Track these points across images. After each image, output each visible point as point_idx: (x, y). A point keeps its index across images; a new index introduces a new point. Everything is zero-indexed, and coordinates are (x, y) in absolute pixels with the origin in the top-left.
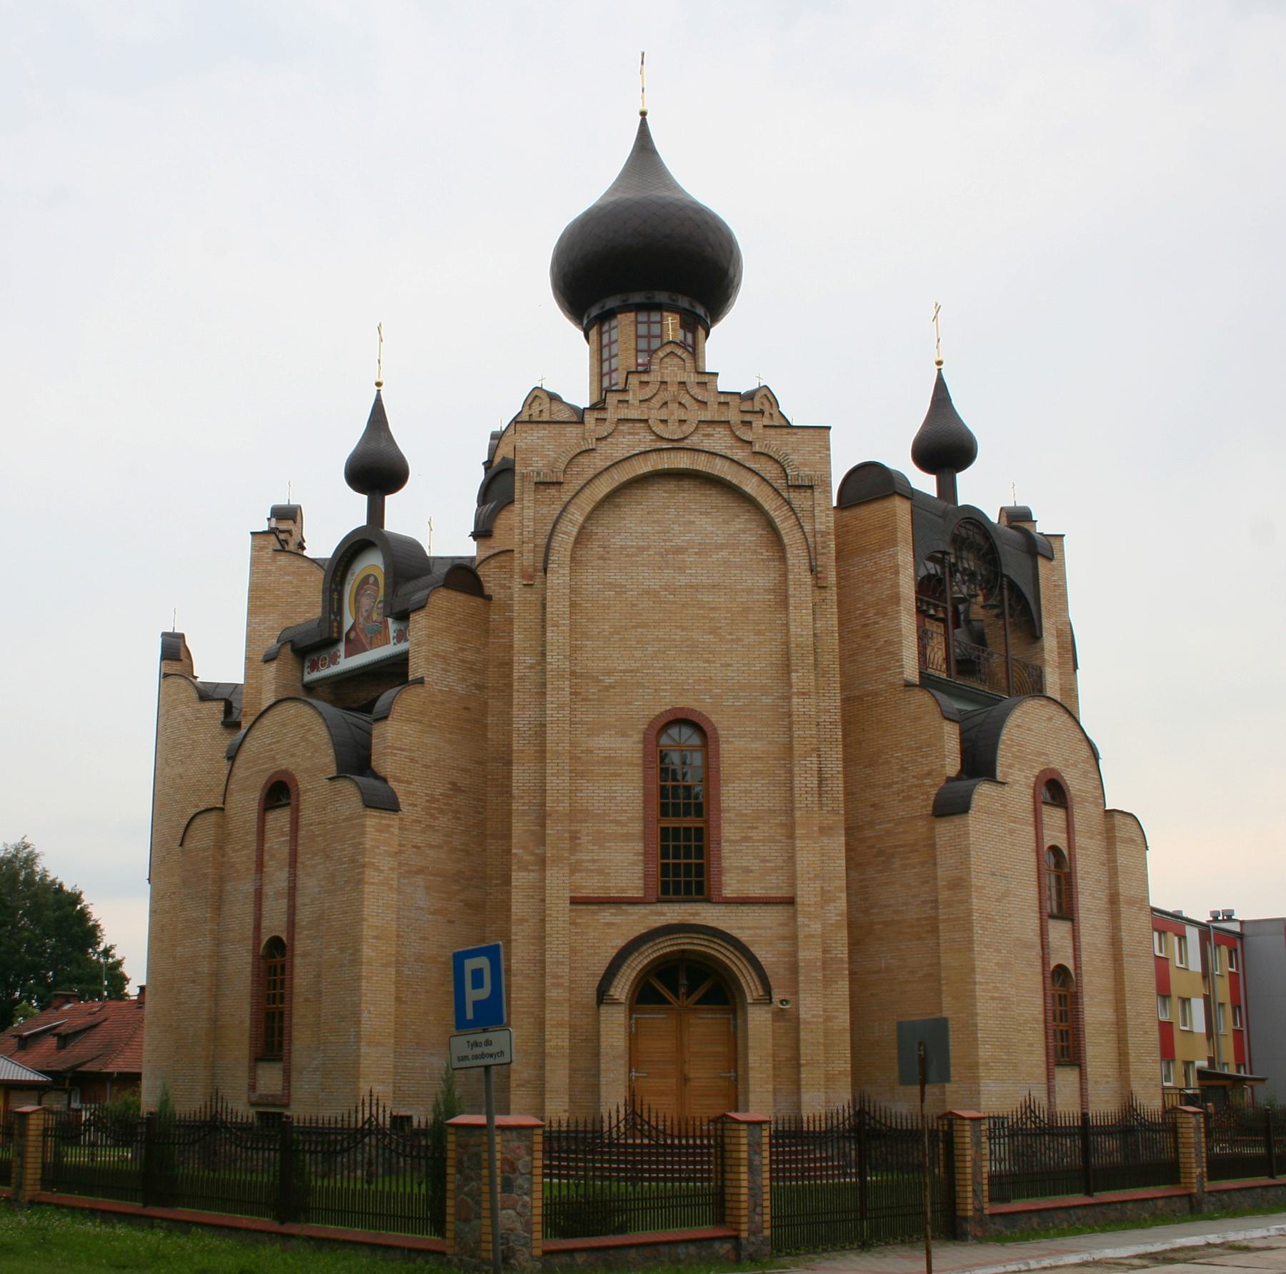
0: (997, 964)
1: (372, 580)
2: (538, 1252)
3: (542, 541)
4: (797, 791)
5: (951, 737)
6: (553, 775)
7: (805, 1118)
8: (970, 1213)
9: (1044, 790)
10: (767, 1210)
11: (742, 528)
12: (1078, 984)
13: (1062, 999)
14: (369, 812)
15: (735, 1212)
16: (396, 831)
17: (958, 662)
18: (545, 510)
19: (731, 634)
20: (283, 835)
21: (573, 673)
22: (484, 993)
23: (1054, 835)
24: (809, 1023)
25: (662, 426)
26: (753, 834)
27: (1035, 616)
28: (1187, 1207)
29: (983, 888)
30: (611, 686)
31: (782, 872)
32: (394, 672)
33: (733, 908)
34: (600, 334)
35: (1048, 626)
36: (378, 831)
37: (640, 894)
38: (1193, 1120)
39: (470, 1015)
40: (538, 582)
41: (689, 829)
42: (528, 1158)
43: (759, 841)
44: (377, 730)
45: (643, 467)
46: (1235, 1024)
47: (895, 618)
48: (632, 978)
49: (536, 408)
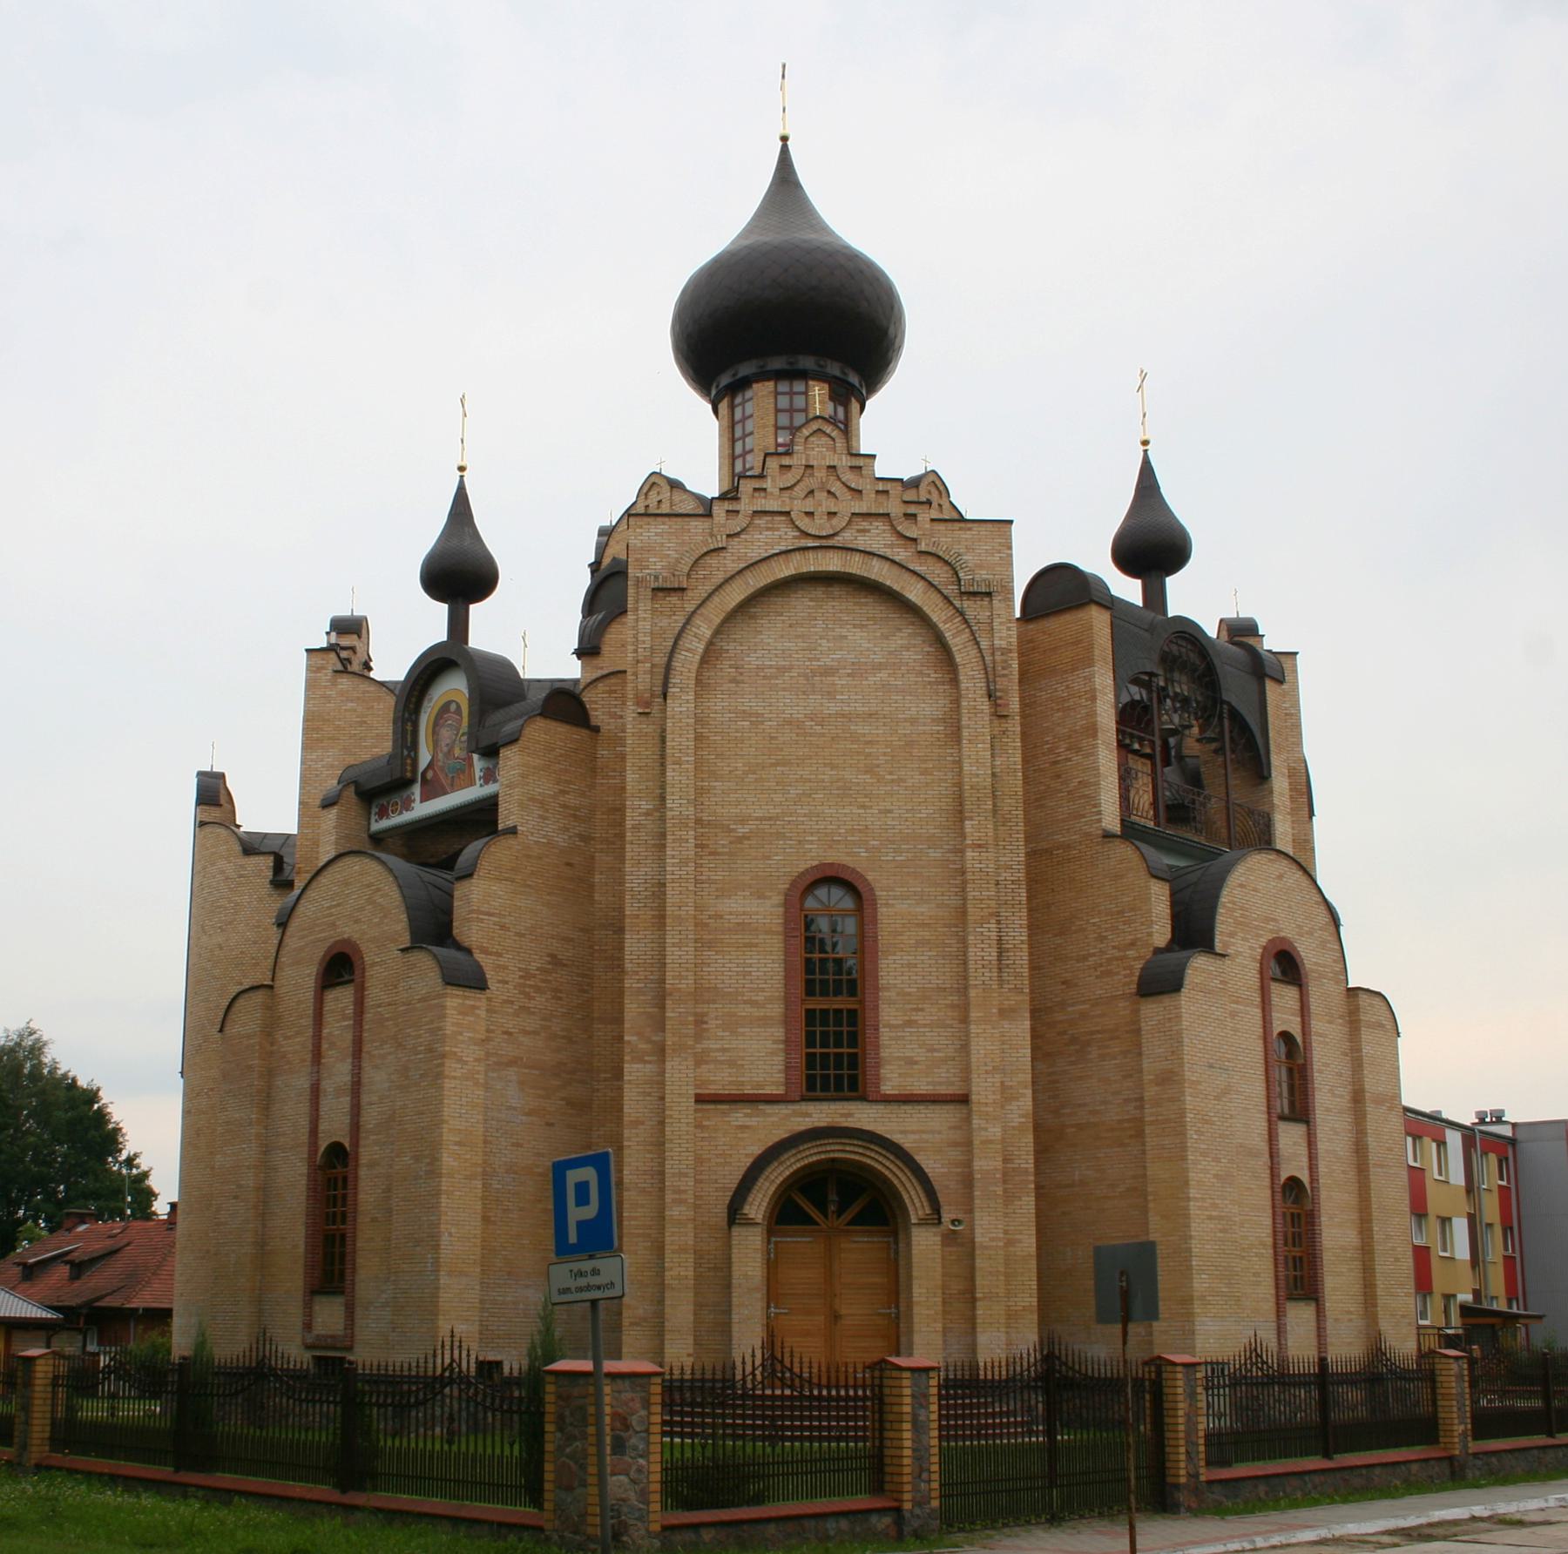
0: (1216, 1176)
1: (453, 707)
2: (656, 1527)
3: (660, 660)
4: (971, 965)
5: (1159, 899)
6: (674, 945)
7: (981, 1364)
8: (1183, 1480)
9: (1273, 964)
10: (935, 1476)
11: (905, 644)
12: (1315, 1200)
13: (1295, 1219)
14: (450, 990)
15: (896, 1478)
16: (483, 1013)
17: (1168, 807)
18: (664, 622)
19: (891, 773)
20: (345, 1018)
21: (698, 821)
22: (590, 1211)
23: (1286, 1019)
24: (986, 1248)
25: (807, 520)
26: (918, 1017)
27: (1262, 751)
28: (1447, 1472)
29: (1199, 1083)
30: (745, 837)
31: (954, 1064)
32: (480, 819)
33: (894, 1107)
34: (732, 407)
35: (1278, 763)
36: (460, 1013)
37: (781, 1090)
38: (1455, 1366)
39: (573, 1238)
40: (655, 709)
41: (841, 1011)
42: (643, 1413)
43: (925, 1026)
44: (460, 890)
45: (784, 570)
46: (1506, 1249)
47: (1092, 753)
48: (770, 1193)
49: (653, 497)
